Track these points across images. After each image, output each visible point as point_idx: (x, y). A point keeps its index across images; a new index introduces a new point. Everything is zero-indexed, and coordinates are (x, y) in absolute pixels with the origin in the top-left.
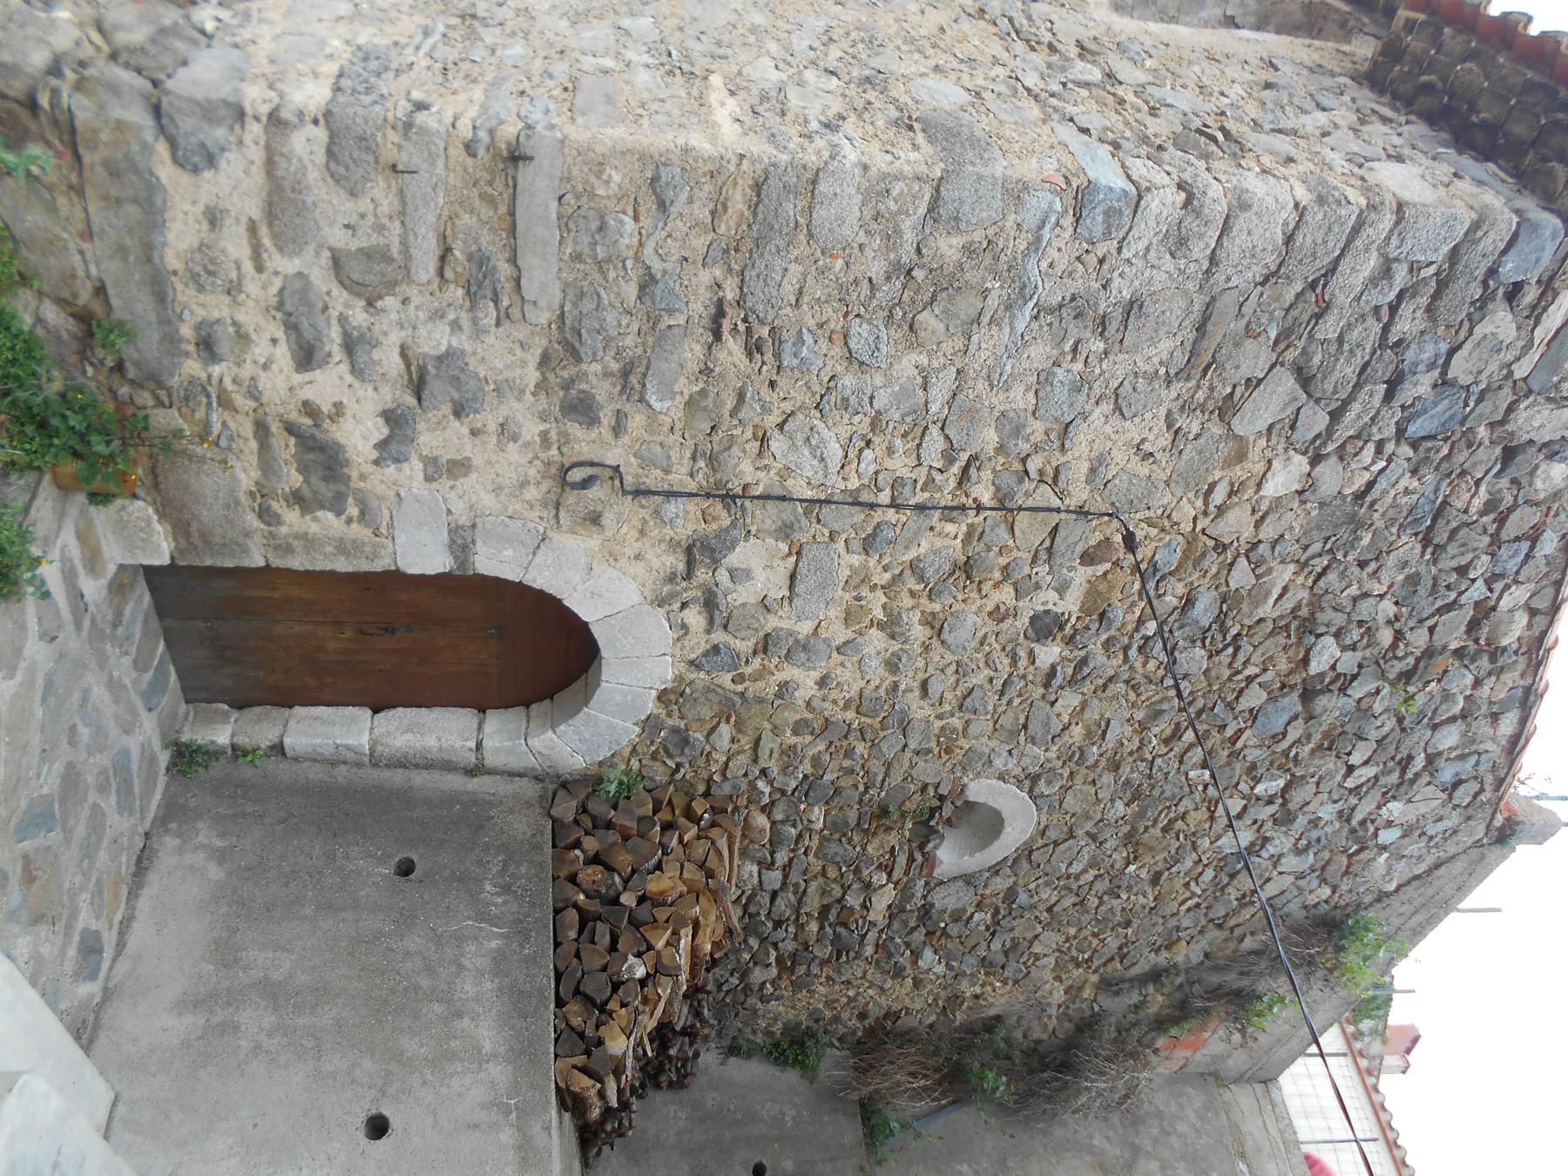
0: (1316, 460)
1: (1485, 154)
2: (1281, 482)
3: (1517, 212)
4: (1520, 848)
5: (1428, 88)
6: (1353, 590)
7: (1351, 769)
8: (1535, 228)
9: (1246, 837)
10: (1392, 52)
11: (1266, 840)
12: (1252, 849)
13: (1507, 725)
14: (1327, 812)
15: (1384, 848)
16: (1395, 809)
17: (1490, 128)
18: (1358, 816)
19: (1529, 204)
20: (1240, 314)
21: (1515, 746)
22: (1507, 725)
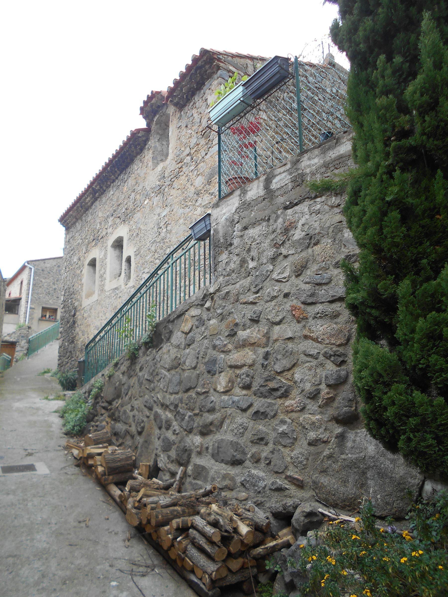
0: (260, 110)
1: (203, 84)
2: (264, 116)
3: (218, 78)
4: (335, 61)
5: (187, 96)
6: (283, 102)
7: (319, 99)
8: (221, 75)
9: (336, 121)
10: (176, 105)
11: (337, 117)
12: (340, 120)
13: (307, 67)
14: (329, 104)
15: (337, 91)
16: (328, 90)
17: (198, 83)
18: (330, 97)
19: (215, 76)
20: (129, 260)
21: (312, 65)
22: (307, 67)
